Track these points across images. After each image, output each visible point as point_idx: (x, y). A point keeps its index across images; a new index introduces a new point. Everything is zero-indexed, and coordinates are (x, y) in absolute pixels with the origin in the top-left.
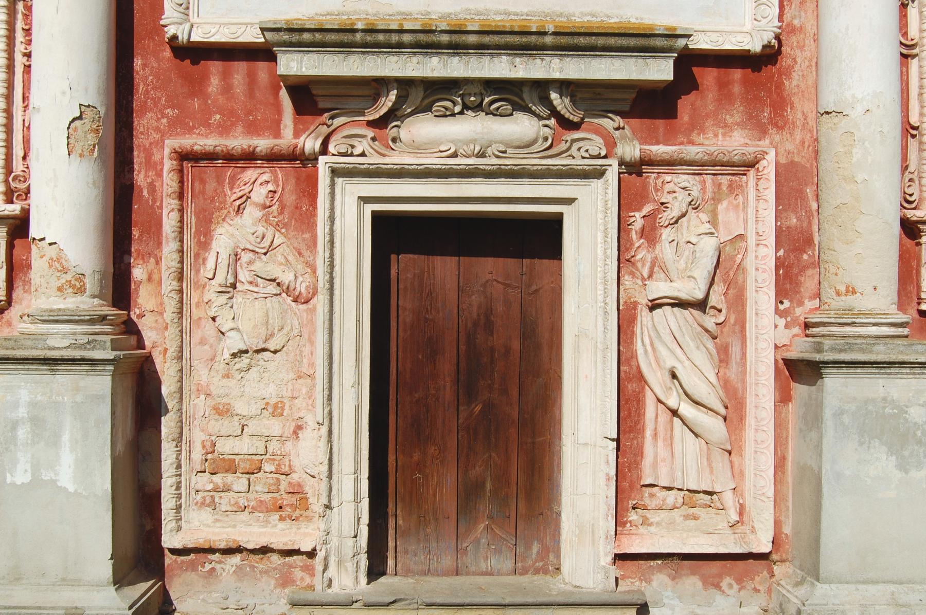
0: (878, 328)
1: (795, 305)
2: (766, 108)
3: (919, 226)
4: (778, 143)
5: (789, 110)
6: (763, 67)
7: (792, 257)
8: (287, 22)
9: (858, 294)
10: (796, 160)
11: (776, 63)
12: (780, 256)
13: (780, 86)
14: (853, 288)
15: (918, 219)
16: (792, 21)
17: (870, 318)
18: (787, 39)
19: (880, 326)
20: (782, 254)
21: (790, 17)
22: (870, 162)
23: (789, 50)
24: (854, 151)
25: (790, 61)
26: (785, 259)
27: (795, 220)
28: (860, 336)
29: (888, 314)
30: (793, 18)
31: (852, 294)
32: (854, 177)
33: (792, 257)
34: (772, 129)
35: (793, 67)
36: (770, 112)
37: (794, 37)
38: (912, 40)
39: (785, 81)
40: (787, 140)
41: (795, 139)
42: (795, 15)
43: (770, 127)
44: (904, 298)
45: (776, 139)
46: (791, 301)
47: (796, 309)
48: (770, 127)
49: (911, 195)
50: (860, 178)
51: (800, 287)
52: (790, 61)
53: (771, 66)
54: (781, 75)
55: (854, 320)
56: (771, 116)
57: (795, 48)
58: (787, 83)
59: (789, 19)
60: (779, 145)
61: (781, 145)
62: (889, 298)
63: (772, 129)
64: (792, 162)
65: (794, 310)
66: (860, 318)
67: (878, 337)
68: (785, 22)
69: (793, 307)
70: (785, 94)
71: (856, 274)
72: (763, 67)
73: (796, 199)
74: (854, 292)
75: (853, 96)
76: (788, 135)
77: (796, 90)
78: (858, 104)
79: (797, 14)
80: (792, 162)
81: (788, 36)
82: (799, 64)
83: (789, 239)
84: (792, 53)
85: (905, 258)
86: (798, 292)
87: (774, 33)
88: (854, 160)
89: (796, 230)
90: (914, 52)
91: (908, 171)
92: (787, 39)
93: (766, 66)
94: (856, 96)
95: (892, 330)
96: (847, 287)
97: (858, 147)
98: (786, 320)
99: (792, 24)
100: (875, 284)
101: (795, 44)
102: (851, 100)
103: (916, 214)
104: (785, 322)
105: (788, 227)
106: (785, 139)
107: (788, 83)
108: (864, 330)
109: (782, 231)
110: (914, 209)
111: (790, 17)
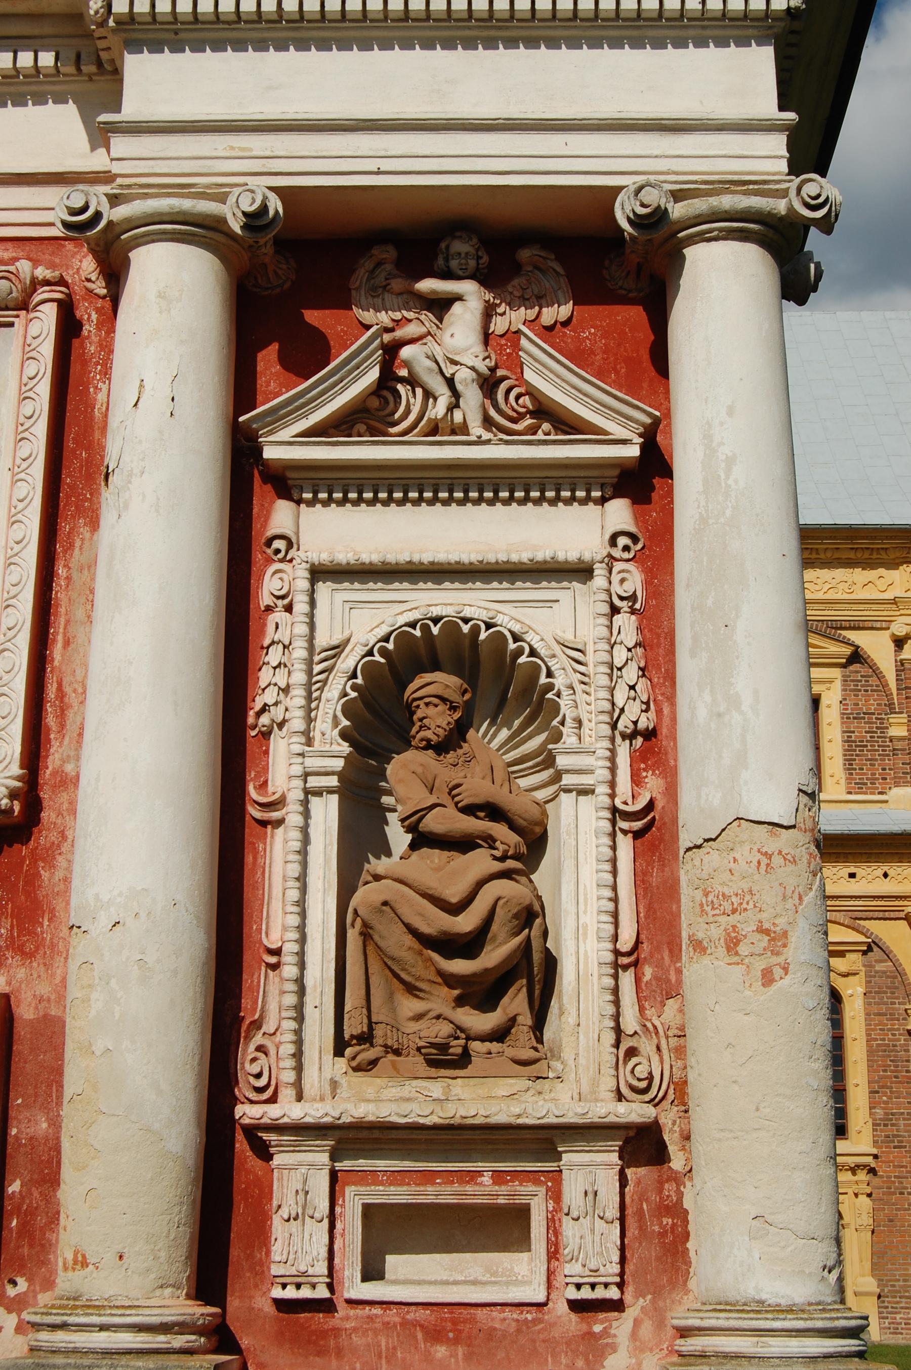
0: (112, 1334)
1: (38, 1288)
2: (3, 919)
3: (260, 1134)
4: (21, 983)
5: (46, 923)
6: (5, 847)
7: (36, 1194)
8: (70, 782)
9: (91, 1266)
10: (53, 1013)
11: (29, 839)
12: (13, 1192)
13: (33, 879)
14: (84, 1256)
15: (252, 1121)
16: (62, 766)
17: (92, 1314)
18: (50, 798)
19: (115, 1332)
20: (18, 1190)
21: (60, 760)
22: (117, 1018)
23: (53, 816)
24: (94, 996)
25: (54, 837)
26: (23, 1198)
27: (44, 1125)
28: (75, 1351)
29: (139, 1306)
30: (64, 761)
31: (82, 1266)
32: (91, 1045)
33: (36, 1194)
34: (13, 958)
35: (59, 846)
36: (12, 926)
37: (64, 794)
38: (274, 793)
39: (42, 872)
40: (39, 976)
41: (53, 975)
42: (69, 756)
43: (9, 954)
44: (248, 1274)
45: (19, 976)
46: (30, 1280)
47: (40, 1296)
48: (9, 954)
49: (258, 1076)
50: (99, 1047)
51: (48, 1253)
52: (54, 837)
53: (20, 846)
54: (36, 861)
55: (65, 1318)
56: (12, 934)
57: (65, 814)
58: (45, 875)
59: (58, 763)
60: (23, 986)
61: (27, 986)
62: (152, 1276)
63: (13, 958)
64: (46, 1016)
65: (35, 1297)
66: (77, 1315)
67: (107, 1353)
68: (50, 768)
69: (34, 1291)
70: (41, 894)
71: (88, 1228)
72: (5, 847)
73: (50, 1086)
74: (85, 1264)
75: (97, 897)
76: (42, 967)
77: (62, 886)
78: (102, 913)
79: (72, 753)
80: (46, 1016)
81: (53, 792)
82: (69, 841)
83: (32, 1159)
84: (59, 821)
85: (252, 1197)
86: (44, 1263)
87: (7, 788)
88: (93, 1012)
89: (45, 1144)
90: (275, 815)
91: (262, 1031)
92: (50, 798)
93: (11, 846)
94: (101, 897)
95: (139, 1339)
96: (76, 1254)
97: (99, 989)
98: (19, 1316)
99: (63, 771)
100: (119, 1248)
101: (65, 806)
102: (92, 904)
103: (247, 1112)
104: (16, 1320)
105: (31, 1138)
106: (35, 976)
107: (46, 874)
108: (83, 1339)
109: (20, 1145)
110: (267, 1102)
111: (60, 760)
